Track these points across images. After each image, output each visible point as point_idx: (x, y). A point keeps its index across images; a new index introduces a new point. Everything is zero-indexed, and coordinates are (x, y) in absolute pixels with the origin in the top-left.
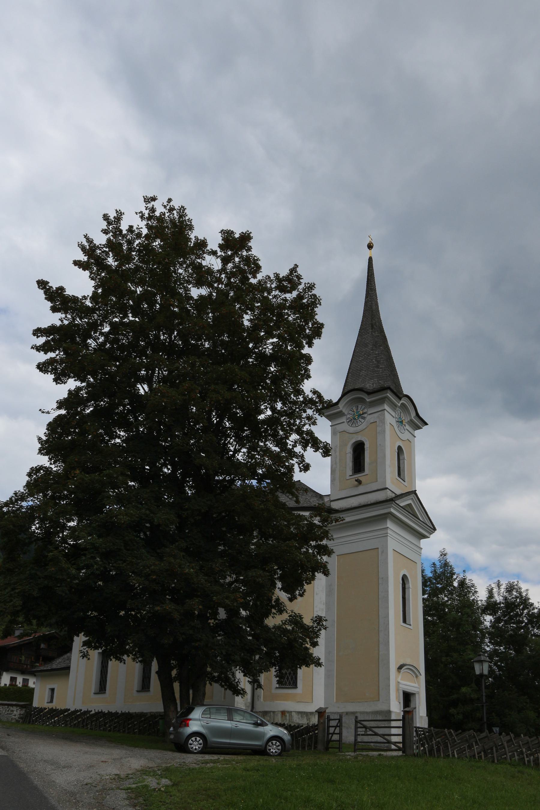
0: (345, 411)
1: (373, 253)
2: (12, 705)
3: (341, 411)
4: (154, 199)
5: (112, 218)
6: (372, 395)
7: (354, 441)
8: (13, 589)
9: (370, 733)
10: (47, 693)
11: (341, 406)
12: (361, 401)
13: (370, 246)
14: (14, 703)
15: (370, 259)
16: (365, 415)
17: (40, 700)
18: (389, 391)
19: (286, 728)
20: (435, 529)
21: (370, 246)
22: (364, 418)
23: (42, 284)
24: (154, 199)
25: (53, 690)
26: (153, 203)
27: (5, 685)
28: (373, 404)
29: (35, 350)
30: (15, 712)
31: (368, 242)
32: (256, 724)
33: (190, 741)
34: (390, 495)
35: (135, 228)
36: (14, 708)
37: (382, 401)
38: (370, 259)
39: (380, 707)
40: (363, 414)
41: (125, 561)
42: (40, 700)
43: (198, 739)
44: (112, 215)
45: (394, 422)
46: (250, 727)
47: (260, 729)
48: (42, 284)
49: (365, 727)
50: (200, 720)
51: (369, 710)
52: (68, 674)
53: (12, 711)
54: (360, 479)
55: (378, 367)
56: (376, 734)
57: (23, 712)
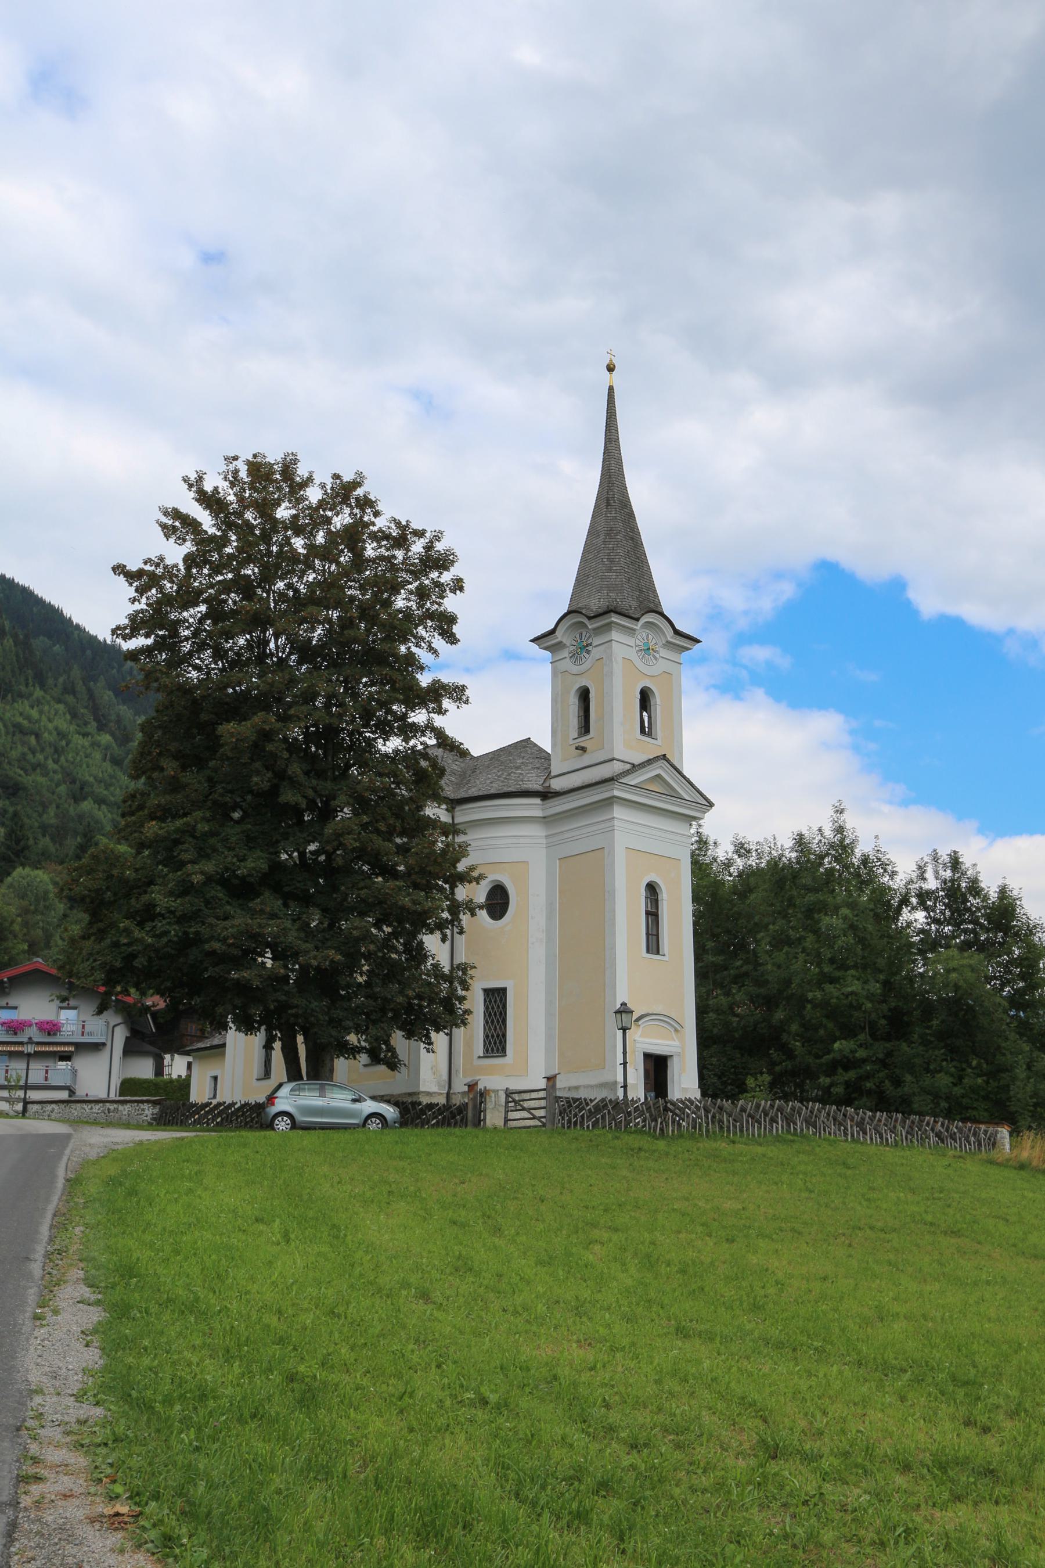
0: (567, 641)
1: (616, 379)
2: (142, 1102)
3: (560, 642)
4: (235, 458)
5: (192, 479)
6: (593, 621)
7: (577, 686)
8: (95, 960)
9: (519, 1107)
10: (208, 1084)
11: (559, 633)
12: (582, 625)
13: (611, 369)
14: (145, 1098)
15: (611, 389)
16: (590, 648)
17: (199, 1094)
18: (613, 614)
19: (388, 1102)
20: (711, 805)
21: (611, 369)
22: (588, 652)
23: (119, 569)
24: (235, 458)
25: (215, 1078)
26: (235, 463)
27: (180, 1076)
28: (598, 631)
29: (192, 494)
30: (147, 1112)
31: (608, 362)
32: (355, 1101)
33: (276, 1122)
34: (618, 767)
35: (220, 490)
36: (145, 1106)
37: (608, 627)
38: (611, 389)
39: (605, 1077)
40: (588, 645)
41: (203, 923)
42: (199, 1094)
43: (285, 1118)
44: (193, 477)
45: (633, 655)
46: (349, 1105)
47: (358, 1105)
48: (119, 569)
49: (514, 1101)
50: (287, 1098)
51: (594, 1082)
52: (223, 1054)
53: (143, 1110)
54: (582, 744)
55: (610, 570)
56: (524, 1109)
57: (156, 1110)
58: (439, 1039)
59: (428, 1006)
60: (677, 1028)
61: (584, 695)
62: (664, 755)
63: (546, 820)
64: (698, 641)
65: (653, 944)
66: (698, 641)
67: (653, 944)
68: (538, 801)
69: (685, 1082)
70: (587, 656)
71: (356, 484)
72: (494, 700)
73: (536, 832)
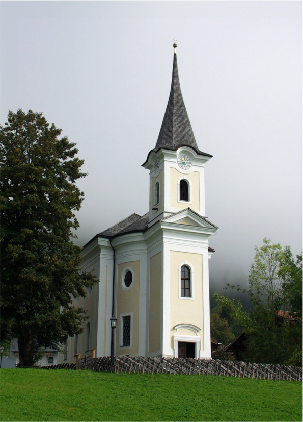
1: (176, 51)
11: (149, 161)
13: (175, 46)
15: (175, 55)
21: (175, 46)
22: (189, 166)
31: (173, 43)
38: (175, 55)
45: (176, 166)
58: (70, 339)
59: (68, 326)
60: (195, 329)
61: (158, 184)
62: (189, 208)
63: (147, 241)
64: (212, 156)
65: (187, 291)
66: (212, 156)
67: (187, 291)
68: (141, 234)
69: (204, 352)
70: (189, 167)
71: (41, 115)
72: (106, 194)
73: (143, 247)
